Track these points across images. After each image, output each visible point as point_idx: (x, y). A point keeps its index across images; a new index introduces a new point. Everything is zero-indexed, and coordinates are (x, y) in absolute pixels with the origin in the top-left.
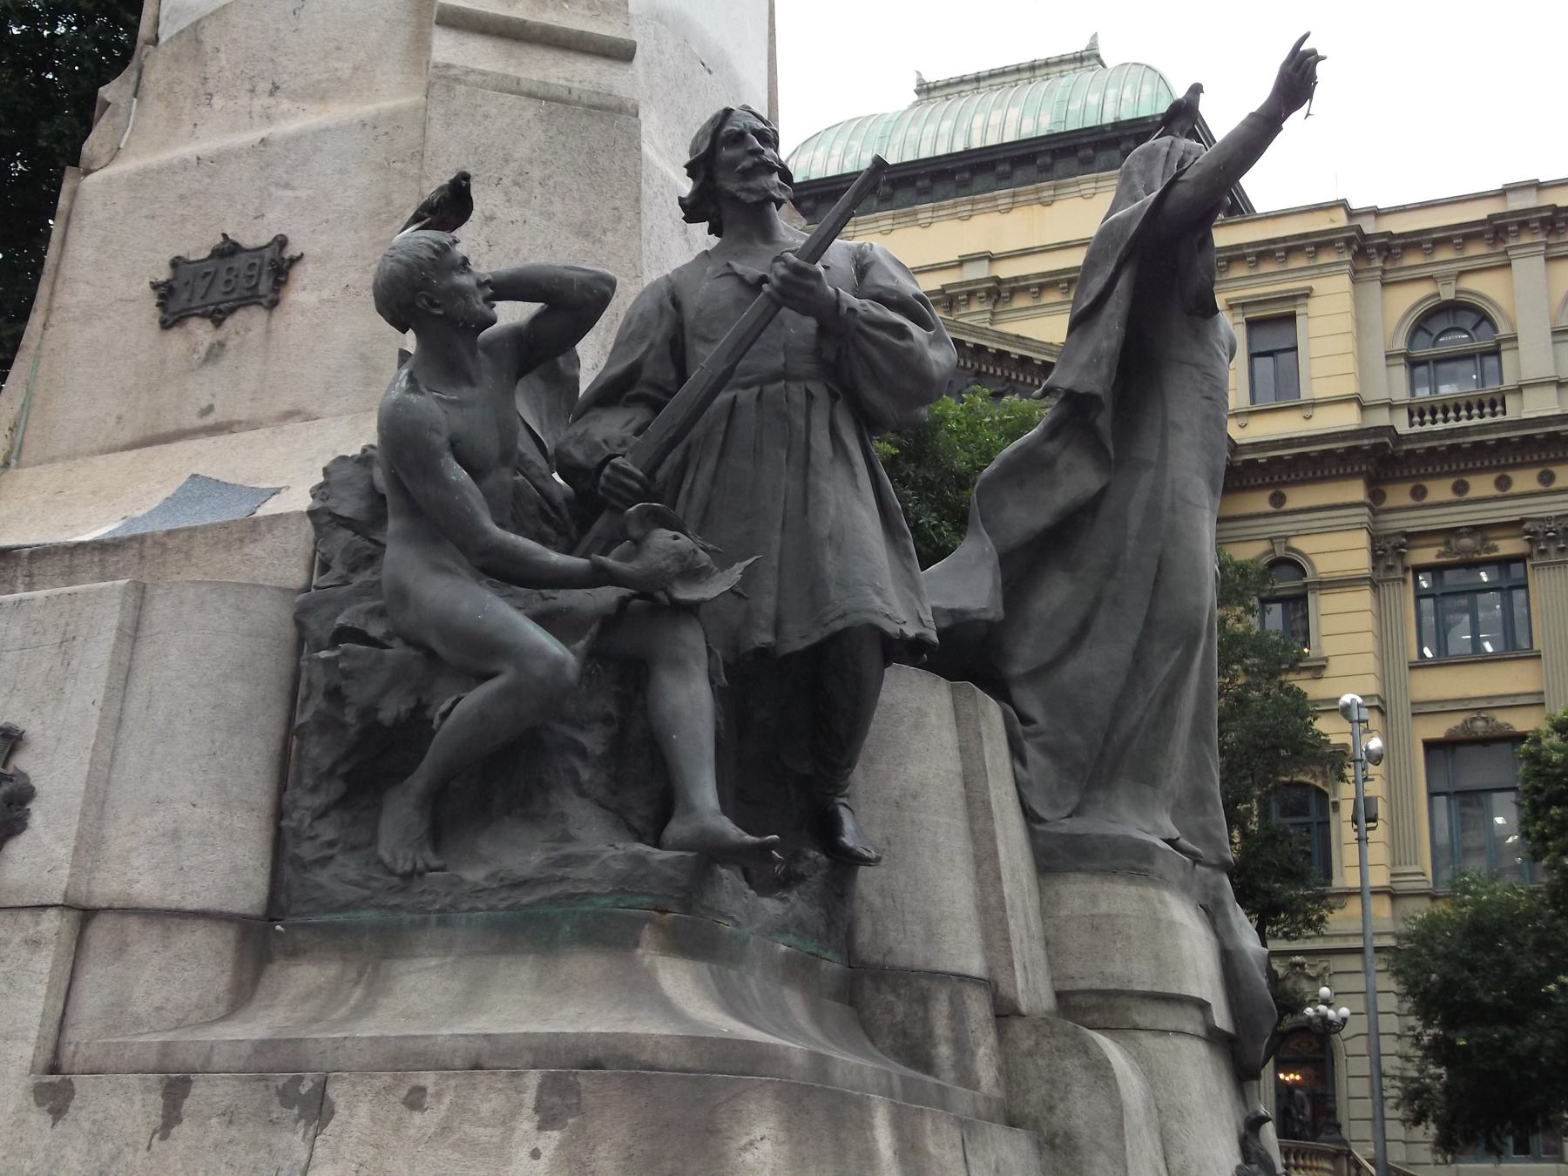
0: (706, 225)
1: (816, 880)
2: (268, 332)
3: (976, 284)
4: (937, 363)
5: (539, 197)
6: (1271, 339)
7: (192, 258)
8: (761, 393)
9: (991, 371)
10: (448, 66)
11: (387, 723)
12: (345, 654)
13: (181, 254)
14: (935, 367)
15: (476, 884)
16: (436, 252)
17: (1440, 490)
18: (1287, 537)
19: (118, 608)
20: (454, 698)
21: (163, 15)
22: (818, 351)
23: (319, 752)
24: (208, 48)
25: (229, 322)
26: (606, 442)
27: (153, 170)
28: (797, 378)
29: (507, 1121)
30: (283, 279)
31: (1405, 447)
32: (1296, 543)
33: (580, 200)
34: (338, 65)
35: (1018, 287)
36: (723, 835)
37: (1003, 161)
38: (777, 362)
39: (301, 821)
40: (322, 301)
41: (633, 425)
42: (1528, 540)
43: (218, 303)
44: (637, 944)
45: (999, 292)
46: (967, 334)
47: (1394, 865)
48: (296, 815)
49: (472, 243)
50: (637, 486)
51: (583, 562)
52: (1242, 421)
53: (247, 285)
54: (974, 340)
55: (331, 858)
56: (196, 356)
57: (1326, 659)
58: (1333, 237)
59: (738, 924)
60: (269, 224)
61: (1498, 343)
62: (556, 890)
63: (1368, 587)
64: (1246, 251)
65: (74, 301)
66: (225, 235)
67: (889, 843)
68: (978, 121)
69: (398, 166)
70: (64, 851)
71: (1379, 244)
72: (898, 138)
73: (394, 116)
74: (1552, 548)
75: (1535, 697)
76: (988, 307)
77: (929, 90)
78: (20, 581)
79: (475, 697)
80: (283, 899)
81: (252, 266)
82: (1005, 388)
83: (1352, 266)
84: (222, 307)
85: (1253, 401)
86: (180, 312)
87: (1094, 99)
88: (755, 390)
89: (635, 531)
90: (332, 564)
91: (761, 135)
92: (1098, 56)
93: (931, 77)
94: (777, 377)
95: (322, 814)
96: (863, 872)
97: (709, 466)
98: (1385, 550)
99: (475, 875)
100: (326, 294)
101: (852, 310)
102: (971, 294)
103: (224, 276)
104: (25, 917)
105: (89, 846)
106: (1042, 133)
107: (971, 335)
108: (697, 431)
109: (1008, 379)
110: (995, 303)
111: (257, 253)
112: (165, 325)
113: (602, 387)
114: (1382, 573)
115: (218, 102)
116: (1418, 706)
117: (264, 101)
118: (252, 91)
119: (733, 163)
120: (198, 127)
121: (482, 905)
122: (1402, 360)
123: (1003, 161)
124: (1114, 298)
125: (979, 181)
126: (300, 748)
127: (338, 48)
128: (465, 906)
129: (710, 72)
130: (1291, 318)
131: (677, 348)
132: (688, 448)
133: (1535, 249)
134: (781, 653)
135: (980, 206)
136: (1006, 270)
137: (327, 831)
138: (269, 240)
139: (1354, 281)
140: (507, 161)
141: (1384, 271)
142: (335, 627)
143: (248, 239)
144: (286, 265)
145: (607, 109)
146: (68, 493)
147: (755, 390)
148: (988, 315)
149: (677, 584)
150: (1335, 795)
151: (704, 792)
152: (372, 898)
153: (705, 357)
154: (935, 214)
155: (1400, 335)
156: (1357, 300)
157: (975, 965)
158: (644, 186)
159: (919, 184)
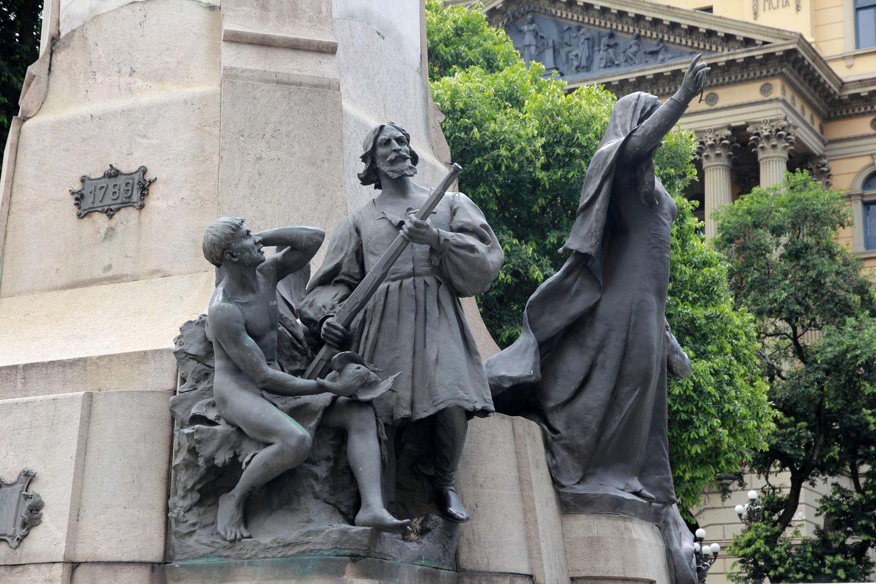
0: (373, 185)
1: (436, 531)
2: (140, 223)
4: (492, 262)
5: (286, 143)
7: (93, 177)
8: (401, 284)
9: (649, 34)
10: (232, 69)
11: (219, 466)
12: (197, 431)
13: (86, 174)
14: (491, 265)
15: (266, 545)
16: (233, 230)
19: (80, 407)
20: (252, 454)
21: (61, 19)
22: (430, 260)
23: (186, 479)
24: (91, 42)
25: (117, 216)
26: (324, 307)
27: (65, 121)
28: (420, 275)
30: (146, 193)
33: (309, 143)
34: (168, 59)
36: (383, 519)
38: (409, 267)
39: (178, 514)
40: (169, 207)
41: (339, 297)
43: (110, 205)
44: (344, 574)
46: (629, 6)
48: (175, 511)
49: (250, 174)
50: (340, 334)
51: (315, 382)
53: (126, 196)
55: (195, 531)
56: (99, 236)
59: (395, 559)
60: (136, 159)
62: (304, 548)
65: (25, 198)
66: (111, 166)
67: (477, 506)
69: (207, 129)
70: (62, 534)
73: (203, 98)
78: (19, 381)
79: (264, 454)
80: (171, 552)
81: (127, 184)
82: (658, 48)
84: (112, 207)
85: (858, 46)
86: (89, 209)
88: (399, 282)
89: (337, 366)
90: (187, 379)
91: (399, 140)
94: (408, 276)
95: (189, 510)
96: (461, 525)
99: (265, 540)
100: (171, 203)
101: (446, 240)
103: (111, 189)
104: (44, 568)
105: (73, 531)
107: (632, 7)
108: (370, 304)
109: (662, 40)
111: (130, 177)
112: (80, 216)
113: (321, 277)
115: (99, 77)
117: (125, 80)
118: (119, 72)
119: (385, 156)
120: (89, 93)
121: (269, 555)
124: (600, 198)
126: (176, 475)
127: (168, 49)
128: (262, 556)
129: (383, 38)
132: (366, 312)
134: (415, 419)
137: (192, 518)
138: (137, 169)
140: (267, 124)
142: (191, 415)
143: (124, 168)
144: (147, 184)
145: (323, 86)
146: (32, 315)
147: (399, 282)
149: (360, 391)
152: (215, 552)
153: (373, 264)
158: (345, 131)
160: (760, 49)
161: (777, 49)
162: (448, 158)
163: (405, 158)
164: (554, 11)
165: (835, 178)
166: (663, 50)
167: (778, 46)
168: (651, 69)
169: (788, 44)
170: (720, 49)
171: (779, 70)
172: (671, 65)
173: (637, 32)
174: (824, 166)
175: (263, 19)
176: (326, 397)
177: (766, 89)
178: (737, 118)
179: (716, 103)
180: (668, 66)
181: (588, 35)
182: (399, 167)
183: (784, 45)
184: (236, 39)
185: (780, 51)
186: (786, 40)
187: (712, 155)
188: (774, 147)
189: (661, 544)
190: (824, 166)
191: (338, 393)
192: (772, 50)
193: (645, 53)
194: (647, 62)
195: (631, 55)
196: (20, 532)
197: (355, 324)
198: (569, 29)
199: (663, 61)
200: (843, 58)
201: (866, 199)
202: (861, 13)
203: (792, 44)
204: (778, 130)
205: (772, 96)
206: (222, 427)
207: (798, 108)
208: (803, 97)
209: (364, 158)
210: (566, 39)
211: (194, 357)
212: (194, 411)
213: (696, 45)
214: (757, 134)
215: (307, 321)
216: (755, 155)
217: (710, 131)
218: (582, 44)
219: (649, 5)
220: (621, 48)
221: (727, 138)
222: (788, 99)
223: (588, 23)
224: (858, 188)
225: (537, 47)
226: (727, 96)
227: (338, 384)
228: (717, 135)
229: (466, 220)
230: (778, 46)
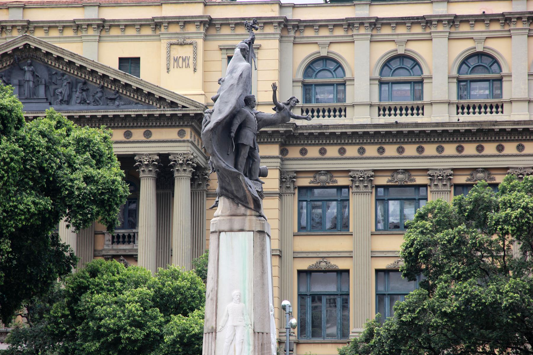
3: (92, 21)
9: (109, 87)
17: (313, 151)
31: (299, 132)
42: (351, 180)
47: (281, 328)
58: (272, 21)
61: (345, 81)
63: (278, 198)
64: (230, 22)
71: (293, 24)
74: (361, 185)
75: (349, 253)
76: (97, 33)
98: (286, 179)
109: (118, 92)
114: (284, 190)
116: (296, 254)
122: (300, 84)
133: (366, 37)
139: (280, 41)
141: (295, 38)
155: (300, 71)
156: (281, 50)
160: (180, 110)
161: (191, 112)
164: (46, 60)
165: (212, 181)
166: (118, 98)
167: (191, 110)
168: (112, 112)
169: (198, 110)
171: (190, 123)
172: (125, 111)
173: (102, 83)
174: (206, 175)
178: (164, 149)
179: (150, 137)
181: (69, 81)
183: (195, 110)
185: (193, 113)
186: (197, 107)
187: (146, 170)
188: (185, 170)
190: (206, 175)
192: (188, 112)
193: (107, 98)
194: (108, 104)
195: (97, 98)
198: (56, 73)
203: (200, 110)
204: (188, 160)
213: (140, 99)
214: (175, 161)
216: (172, 173)
217: (147, 155)
218: (65, 86)
219: (112, 70)
220: (91, 93)
221: (156, 161)
223: (69, 72)
225: (33, 82)
226: (158, 134)
228: (150, 158)
230: (191, 110)
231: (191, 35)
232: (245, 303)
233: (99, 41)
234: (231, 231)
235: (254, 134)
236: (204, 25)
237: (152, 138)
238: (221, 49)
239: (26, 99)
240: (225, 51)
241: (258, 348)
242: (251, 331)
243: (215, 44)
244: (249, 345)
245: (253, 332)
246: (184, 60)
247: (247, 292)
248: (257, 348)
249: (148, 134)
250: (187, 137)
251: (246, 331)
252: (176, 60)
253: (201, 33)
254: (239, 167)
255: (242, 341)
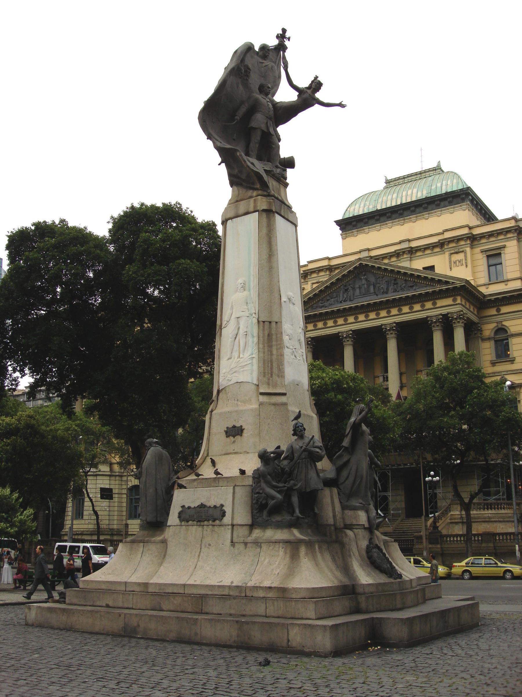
6: (493, 261)
18: (502, 322)
23: (256, 506)
25: (236, 437)
29: (279, 548)
32: (504, 323)
35: (418, 249)
37: (413, 206)
38: (304, 457)
45: (412, 252)
52: (487, 286)
54: (404, 271)
57: (515, 358)
68: (404, 193)
72: (380, 200)
77: (389, 182)
83: (517, 237)
85: (490, 281)
87: (439, 185)
91: (301, 426)
92: (440, 169)
93: (389, 178)
94: (304, 459)
97: (297, 470)
102: (404, 252)
103: (234, 431)
104: (227, 526)
105: (233, 518)
106: (424, 197)
109: (415, 281)
110: (411, 255)
112: (227, 437)
117: (236, 402)
119: (298, 430)
123: (413, 206)
125: (406, 213)
130: (500, 254)
131: (292, 453)
135: (406, 221)
136: (414, 244)
148: (409, 258)
150: (519, 398)
151: (297, 511)
153: (296, 455)
154: (393, 224)
157: (332, 523)
159: (387, 215)
160: (451, 285)
161: (458, 285)
162: (316, 413)
163: (302, 431)
165: (484, 331)
170: (437, 285)
171: (459, 293)
173: (405, 278)
174: (479, 327)
175: (269, 388)
176: (286, 488)
177: (455, 300)
178: (444, 311)
180: (417, 292)
181: (386, 280)
182: (301, 433)
184: (262, 394)
187: (435, 325)
189: (367, 515)
190: (479, 327)
191: (288, 487)
192: (456, 285)
196: (221, 518)
197: (292, 469)
198: (379, 277)
199: (415, 290)
200: (485, 285)
201: (496, 339)
202: (490, 267)
204: (460, 316)
205: (457, 303)
206: (263, 495)
207: (468, 306)
208: (469, 302)
209: (293, 430)
210: (378, 282)
211: (256, 478)
212: (257, 491)
213: (427, 283)
214: (452, 317)
215: (281, 468)
221: (441, 318)
222: (463, 303)
224: (492, 335)
225: (367, 284)
227: (288, 486)
229: (317, 445)
231: (463, 246)
232: (249, 291)
233: (410, 260)
234: (237, 216)
235: (267, 117)
236: (470, 240)
237: (437, 306)
238: (482, 252)
239: (364, 295)
240: (484, 253)
241: (264, 340)
242: (255, 321)
243: (478, 250)
244: (253, 336)
245: (256, 321)
246: (459, 262)
247: (252, 278)
248: (261, 339)
249: (434, 304)
250: (459, 301)
251: (250, 321)
252: (455, 263)
253: (468, 244)
254: (250, 152)
255: (246, 333)
